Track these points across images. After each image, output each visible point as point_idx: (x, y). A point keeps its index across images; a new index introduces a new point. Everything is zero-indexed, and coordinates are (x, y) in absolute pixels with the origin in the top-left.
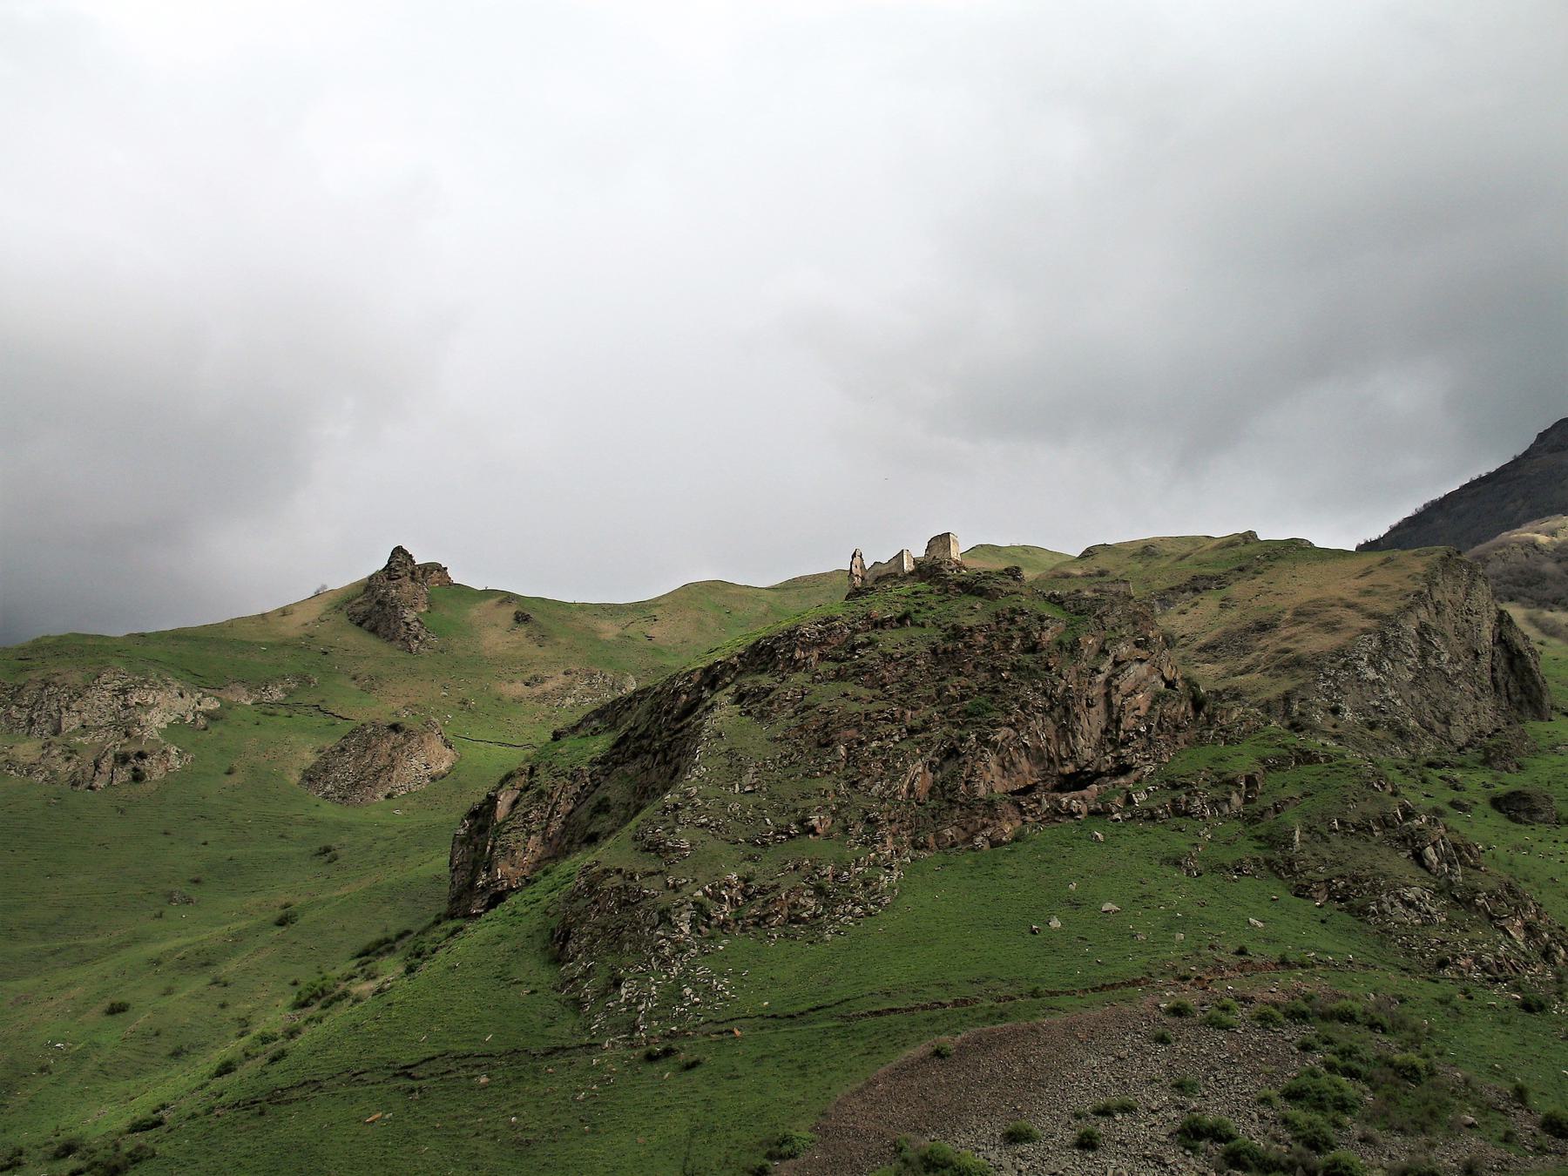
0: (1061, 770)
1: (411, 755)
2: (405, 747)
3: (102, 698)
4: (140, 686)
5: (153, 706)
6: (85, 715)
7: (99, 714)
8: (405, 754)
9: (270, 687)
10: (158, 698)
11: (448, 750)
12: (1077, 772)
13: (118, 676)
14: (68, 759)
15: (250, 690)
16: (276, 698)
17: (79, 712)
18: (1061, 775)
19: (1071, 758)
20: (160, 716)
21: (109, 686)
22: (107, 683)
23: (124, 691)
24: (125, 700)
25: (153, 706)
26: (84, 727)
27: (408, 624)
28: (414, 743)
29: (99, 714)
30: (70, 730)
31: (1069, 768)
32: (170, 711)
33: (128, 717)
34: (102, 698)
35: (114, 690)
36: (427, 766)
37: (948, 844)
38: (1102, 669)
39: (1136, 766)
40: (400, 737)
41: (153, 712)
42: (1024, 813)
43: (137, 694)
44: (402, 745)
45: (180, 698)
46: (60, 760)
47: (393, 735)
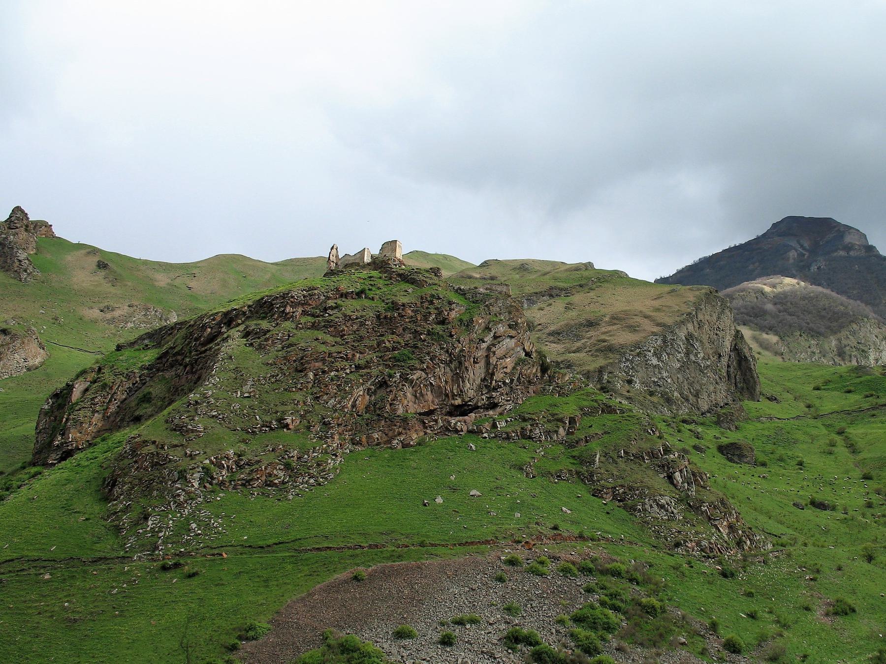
0: (453, 402)
1: (14, 351)
12: (463, 404)
27: (20, 261)
28: (18, 343)
38: (486, 340)
39: (501, 404)
40: (8, 338)
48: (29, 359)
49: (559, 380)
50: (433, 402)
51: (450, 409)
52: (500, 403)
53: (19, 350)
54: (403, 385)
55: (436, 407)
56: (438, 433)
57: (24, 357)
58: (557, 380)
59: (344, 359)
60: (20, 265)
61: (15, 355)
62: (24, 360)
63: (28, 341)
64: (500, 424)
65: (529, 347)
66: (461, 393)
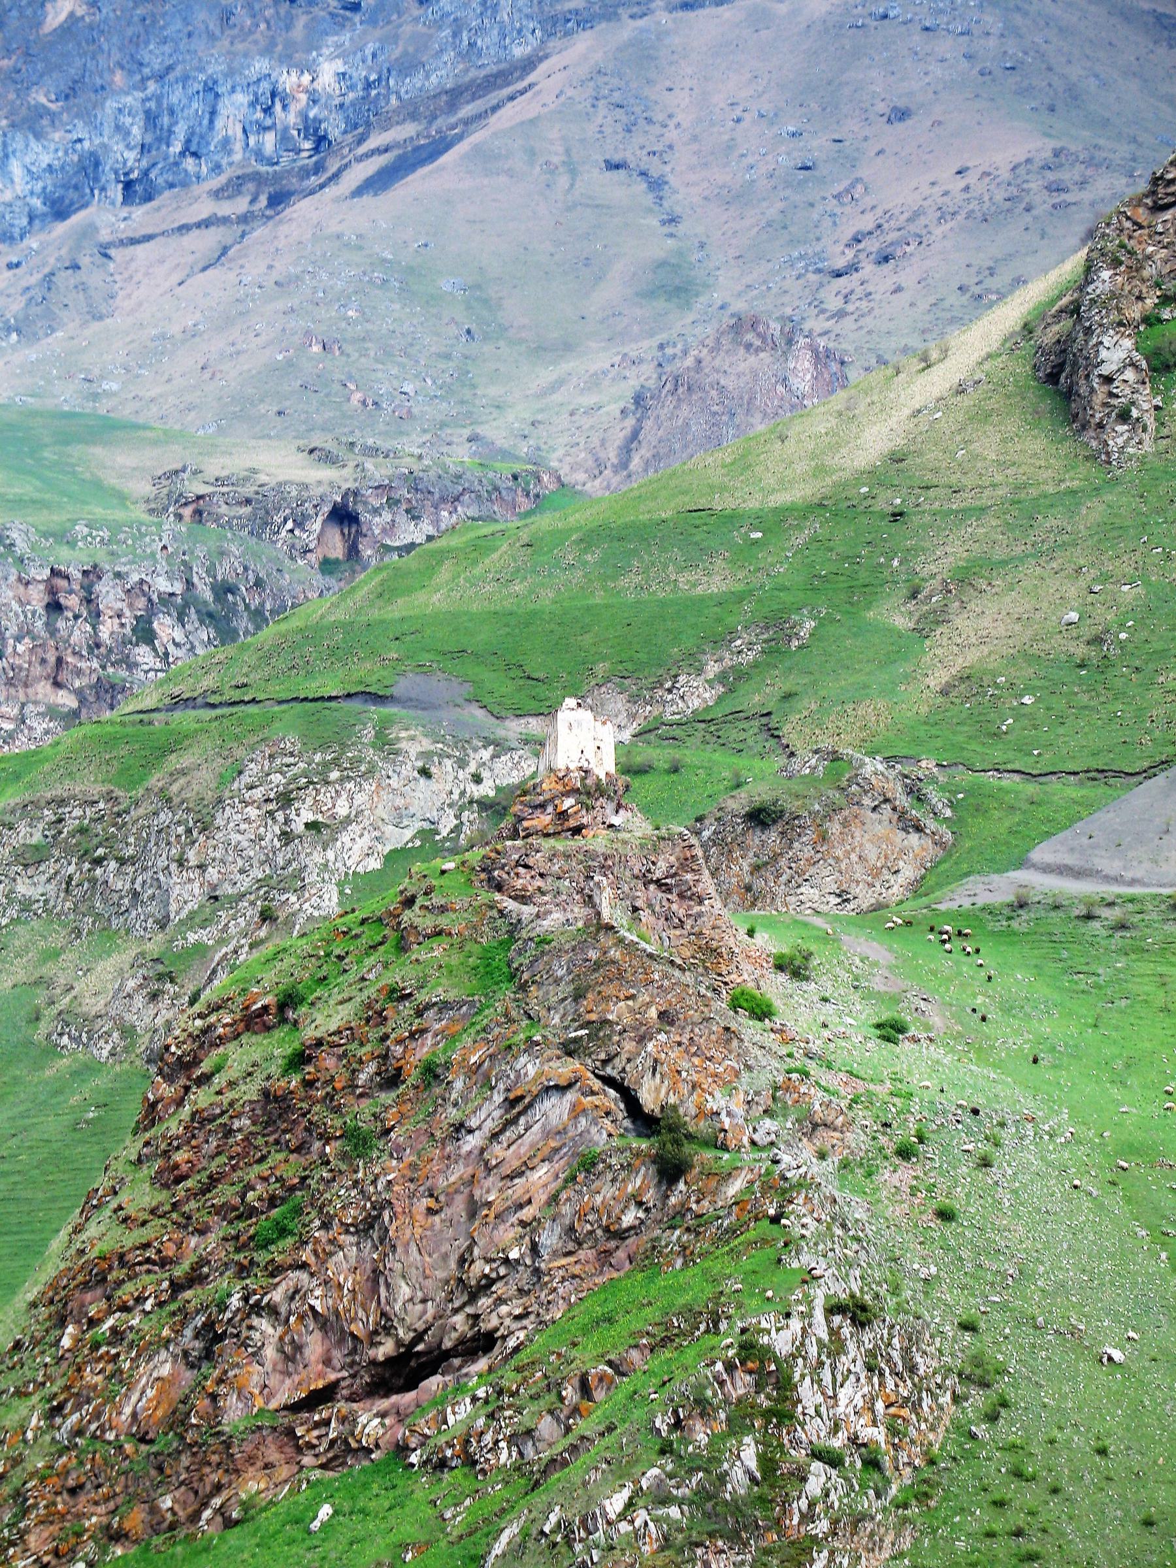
0: (372, 1353)
1: (799, 878)
2: (783, 862)
3: (243, 826)
4: (318, 779)
5: (347, 821)
6: (212, 874)
7: (240, 862)
8: (784, 878)
9: (682, 679)
10: (360, 799)
11: (914, 838)
12: (400, 1356)
13: (278, 761)
14: (154, 997)
15: (634, 699)
16: (695, 703)
17: (202, 867)
18: (373, 1363)
19: (384, 1328)
20: (364, 842)
21: (258, 794)
22: (252, 788)
23: (286, 800)
24: (287, 821)
25: (347, 821)
26: (216, 898)
27: (1108, 380)
28: (803, 849)
29: (240, 862)
30: (183, 915)
31: (385, 1349)
32: (399, 817)
33: (289, 862)
34: (243, 826)
35: (268, 800)
36: (843, 897)
37: (165, 1525)
38: (473, 1123)
39: (499, 1334)
40: (772, 837)
41: (345, 838)
42: (299, 1450)
43: (309, 801)
44: (776, 857)
45: (422, 781)
46: (139, 1001)
47: (755, 838)
48: (856, 890)
49: (705, 1203)
50: (327, 1362)
51: (372, 1376)
52: (497, 1329)
53: (812, 870)
54: (250, 1328)
55: (340, 1375)
56: (330, 1460)
57: (834, 888)
58: (698, 1202)
59: (154, 1263)
60: (1111, 395)
61: (802, 890)
62: (839, 896)
63: (845, 824)
64: (454, 1413)
65: (657, 1090)
66: (386, 1325)
